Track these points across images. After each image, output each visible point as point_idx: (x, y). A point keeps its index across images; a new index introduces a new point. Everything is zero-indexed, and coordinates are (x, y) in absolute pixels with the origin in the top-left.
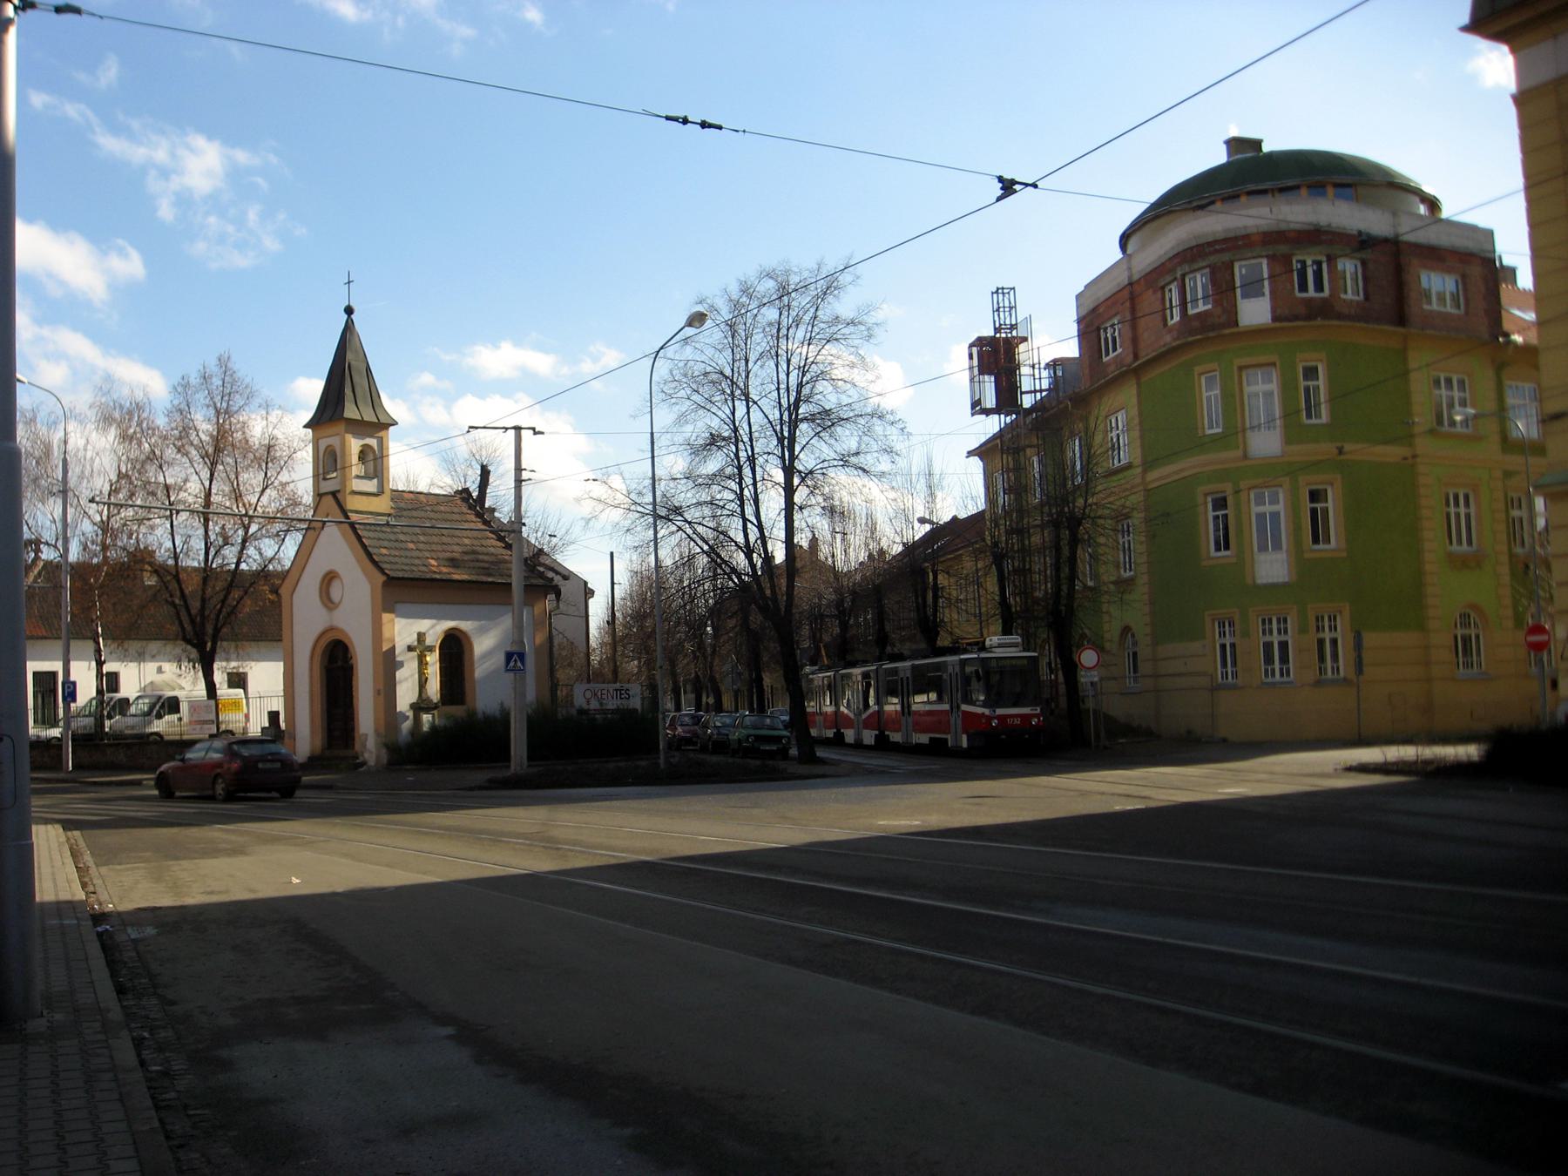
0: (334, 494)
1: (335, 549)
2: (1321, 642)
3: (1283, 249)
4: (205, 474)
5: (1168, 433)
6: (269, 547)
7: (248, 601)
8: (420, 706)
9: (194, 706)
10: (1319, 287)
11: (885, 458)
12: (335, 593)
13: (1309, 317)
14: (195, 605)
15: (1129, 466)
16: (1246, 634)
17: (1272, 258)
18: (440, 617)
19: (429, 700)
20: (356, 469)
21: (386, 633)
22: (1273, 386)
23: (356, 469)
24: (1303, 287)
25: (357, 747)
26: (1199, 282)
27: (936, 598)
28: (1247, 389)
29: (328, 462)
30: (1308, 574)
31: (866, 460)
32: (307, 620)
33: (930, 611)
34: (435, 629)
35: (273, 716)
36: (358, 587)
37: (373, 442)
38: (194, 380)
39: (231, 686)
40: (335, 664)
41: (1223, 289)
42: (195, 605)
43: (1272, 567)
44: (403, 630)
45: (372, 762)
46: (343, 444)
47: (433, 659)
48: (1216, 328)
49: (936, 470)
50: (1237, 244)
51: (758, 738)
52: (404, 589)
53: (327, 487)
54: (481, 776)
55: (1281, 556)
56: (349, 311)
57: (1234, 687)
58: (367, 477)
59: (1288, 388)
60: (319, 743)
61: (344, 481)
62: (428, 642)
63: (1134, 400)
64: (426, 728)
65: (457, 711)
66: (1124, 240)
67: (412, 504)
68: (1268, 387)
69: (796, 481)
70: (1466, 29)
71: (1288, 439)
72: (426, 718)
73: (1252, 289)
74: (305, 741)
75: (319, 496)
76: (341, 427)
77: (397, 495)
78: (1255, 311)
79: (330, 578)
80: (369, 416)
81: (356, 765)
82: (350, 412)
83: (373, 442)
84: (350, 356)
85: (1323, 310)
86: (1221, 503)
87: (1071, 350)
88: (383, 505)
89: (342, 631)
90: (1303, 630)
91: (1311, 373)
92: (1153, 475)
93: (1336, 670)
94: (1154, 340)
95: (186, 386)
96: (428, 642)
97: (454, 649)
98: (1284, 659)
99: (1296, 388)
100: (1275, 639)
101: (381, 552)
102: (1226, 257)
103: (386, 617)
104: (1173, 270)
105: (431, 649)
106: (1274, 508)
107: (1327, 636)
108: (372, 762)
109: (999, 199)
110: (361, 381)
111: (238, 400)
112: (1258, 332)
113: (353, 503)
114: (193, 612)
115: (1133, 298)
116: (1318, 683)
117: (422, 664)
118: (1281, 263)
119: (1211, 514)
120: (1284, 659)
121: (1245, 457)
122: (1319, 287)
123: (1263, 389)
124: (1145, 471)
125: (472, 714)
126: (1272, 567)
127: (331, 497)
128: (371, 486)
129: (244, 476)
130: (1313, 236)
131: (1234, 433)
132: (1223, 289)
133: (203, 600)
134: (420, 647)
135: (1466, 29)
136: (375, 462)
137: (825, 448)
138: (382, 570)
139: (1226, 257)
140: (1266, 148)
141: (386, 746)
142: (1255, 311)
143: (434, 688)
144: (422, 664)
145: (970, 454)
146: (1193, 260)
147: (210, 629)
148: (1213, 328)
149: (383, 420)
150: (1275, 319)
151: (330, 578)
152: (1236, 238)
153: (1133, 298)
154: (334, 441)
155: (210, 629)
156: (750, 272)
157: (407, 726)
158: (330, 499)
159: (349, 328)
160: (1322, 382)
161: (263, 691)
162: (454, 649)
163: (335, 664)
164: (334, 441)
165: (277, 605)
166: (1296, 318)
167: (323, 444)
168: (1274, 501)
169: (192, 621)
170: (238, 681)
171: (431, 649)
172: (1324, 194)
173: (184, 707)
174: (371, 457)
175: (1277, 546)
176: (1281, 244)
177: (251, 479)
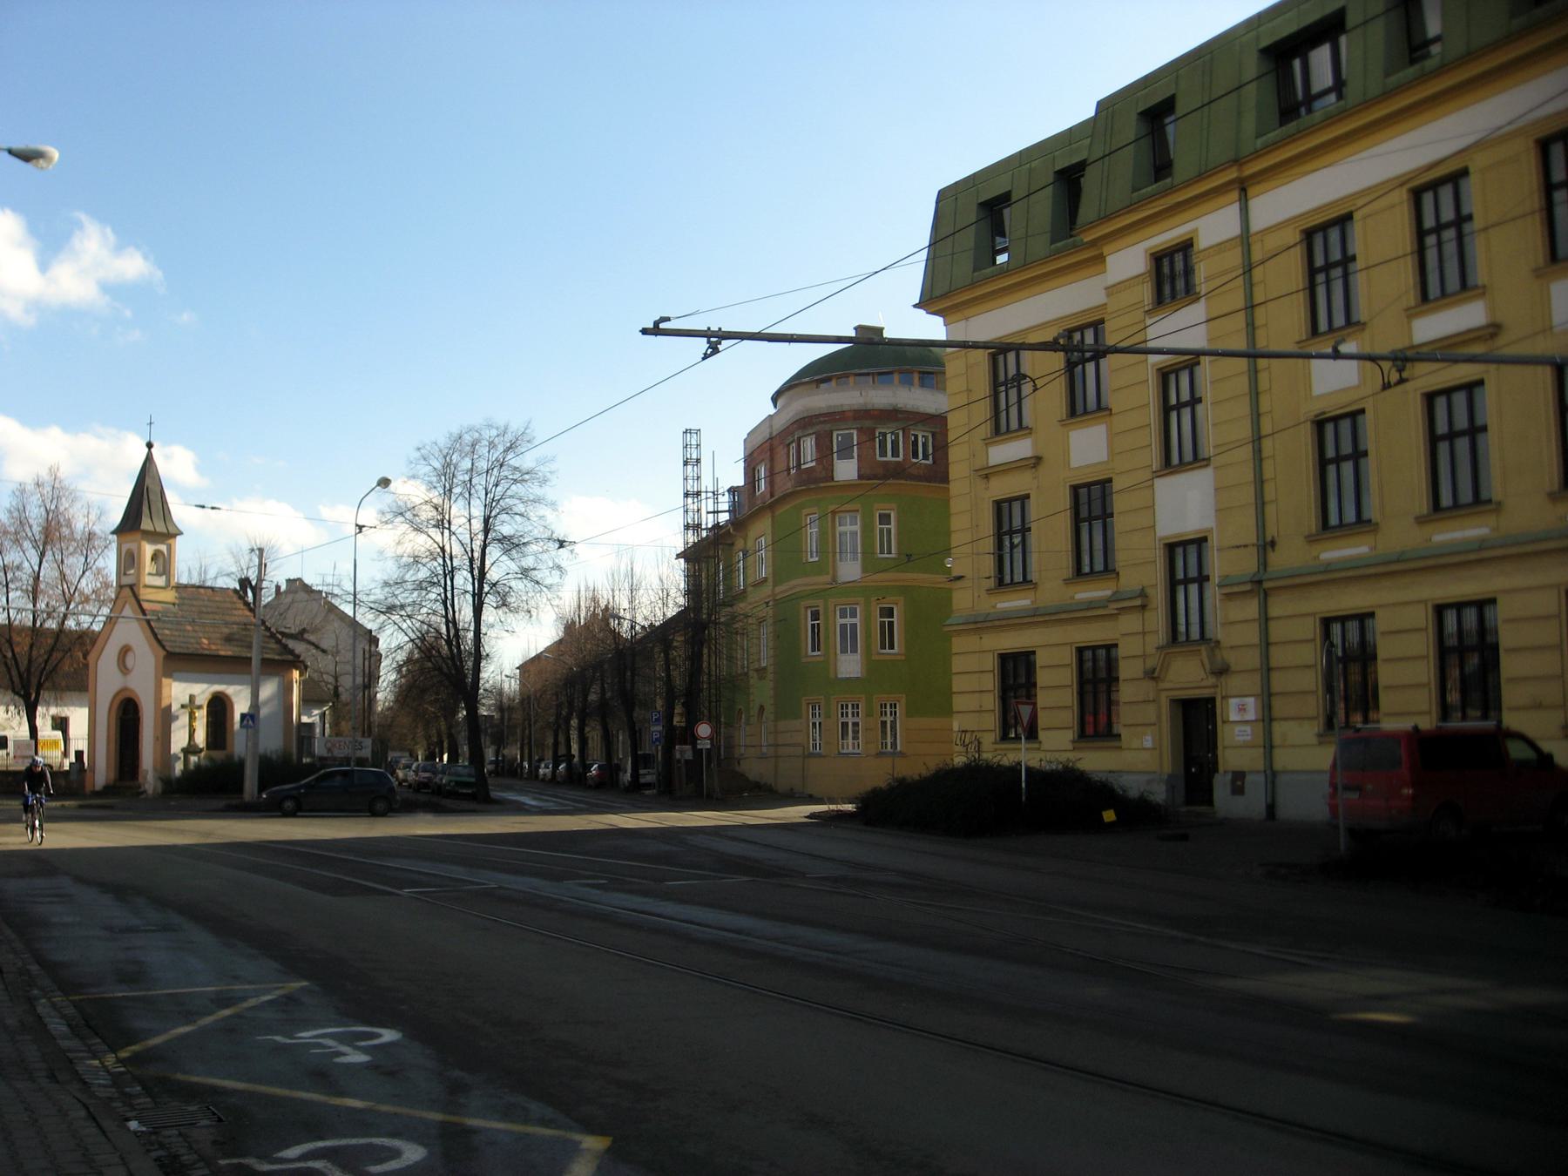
0: (131, 587)
1: (130, 632)
2: (884, 723)
3: (868, 423)
4: (35, 560)
5: (787, 556)
6: (85, 620)
7: (67, 662)
8: (190, 749)
9: (18, 744)
10: (895, 453)
11: (556, 573)
12: (129, 661)
13: (885, 477)
14: (23, 665)
15: (765, 580)
16: (828, 716)
17: (860, 430)
18: (211, 682)
19: (196, 746)
20: (149, 566)
21: (165, 692)
22: (857, 528)
23: (149, 566)
24: (883, 454)
25: (141, 779)
26: (809, 445)
27: (633, 675)
28: (839, 529)
29: (128, 561)
30: (875, 671)
31: (537, 575)
32: (107, 680)
33: (628, 686)
34: (202, 691)
35: (79, 754)
36: (145, 658)
37: (163, 548)
38: (30, 487)
39: (54, 728)
40: (127, 716)
41: (825, 454)
42: (23, 665)
43: (850, 665)
44: (179, 691)
45: (150, 791)
46: (139, 548)
47: (202, 716)
48: (818, 480)
49: (637, 570)
50: (836, 417)
51: (457, 783)
52: (180, 661)
53: (126, 581)
54: (222, 803)
55: (857, 657)
56: (150, 445)
57: (819, 756)
58: (158, 574)
59: (867, 529)
60: (112, 776)
61: (138, 575)
62: (198, 702)
63: (769, 531)
64: (192, 767)
65: (218, 755)
66: (775, 399)
67: (196, 595)
68: (854, 528)
69: (486, 588)
70: (915, 306)
71: (865, 570)
72: (193, 759)
73: (845, 453)
74: (102, 774)
75: (120, 587)
76: (138, 536)
77: (180, 588)
78: (846, 470)
79: (125, 651)
80: (160, 528)
81: (138, 792)
82: (146, 524)
83: (163, 548)
84: (148, 481)
85: (895, 472)
86: (815, 616)
87: (739, 481)
88: (170, 596)
89: (132, 691)
90: (869, 714)
91: (885, 519)
92: (778, 589)
93: (894, 745)
94: (785, 485)
95: (23, 492)
96: (198, 702)
97: (219, 706)
98: (856, 732)
99: (873, 530)
100: (850, 720)
101: (165, 633)
102: (827, 427)
103: (165, 681)
104: (792, 433)
105: (200, 707)
106: (853, 620)
107: (889, 719)
108: (150, 791)
109: (706, 357)
110: (157, 506)
111: (65, 504)
112: (847, 486)
113: (145, 594)
114: (22, 669)
115: (772, 450)
116: (880, 754)
117: (192, 717)
118: (868, 435)
119: (810, 623)
120: (856, 732)
121: (834, 579)
122: (895, 453)
123: (850, 527)
124: (775, 585)
125: (230, 757)
126: (850, 665)
127: (129, 590)
128: (161, 581)
129: (69, 561)
130: (892, 415)
131: (826, 563)
132: (825, 454)
133: (30, 661)
134: (191, 706)
135: (915, 306)
136: (164, 563)
137: (509, 563)
138: (163, 647)
139: (827, 427)
140: (886, 335)
141: (161, 779)
142: (846, 470)
143: (201, 738)
144: (192, 717)
145: (678, 556)
146: (804, 427)
147: (34, 681)
148: (817, 481)
149: (171, 530)
150: (860, 477)
151: (125, 651)
152: (834, 413)
153: (772, 450)
154: (133, 546)
155: (34, 681)
156: (476, 420)
157: (179, 767)
158: (127, 591)
159: (149, 459)
160: (893, 526)
161: (72, 731)
162: (219, 706)
163: (127, 716)
164: (133, 546)
165: (86, 666)
166: (875, 477)
167: (125, 548)
168: (854, 615)
169: (20, 676)
170: (61, 724)
171: (200, 707)
172: (911, 384)
173: (10, 744)
174: (161, 560)
175: (854, 651)
176: (869, 419)
177: (75, 563)
